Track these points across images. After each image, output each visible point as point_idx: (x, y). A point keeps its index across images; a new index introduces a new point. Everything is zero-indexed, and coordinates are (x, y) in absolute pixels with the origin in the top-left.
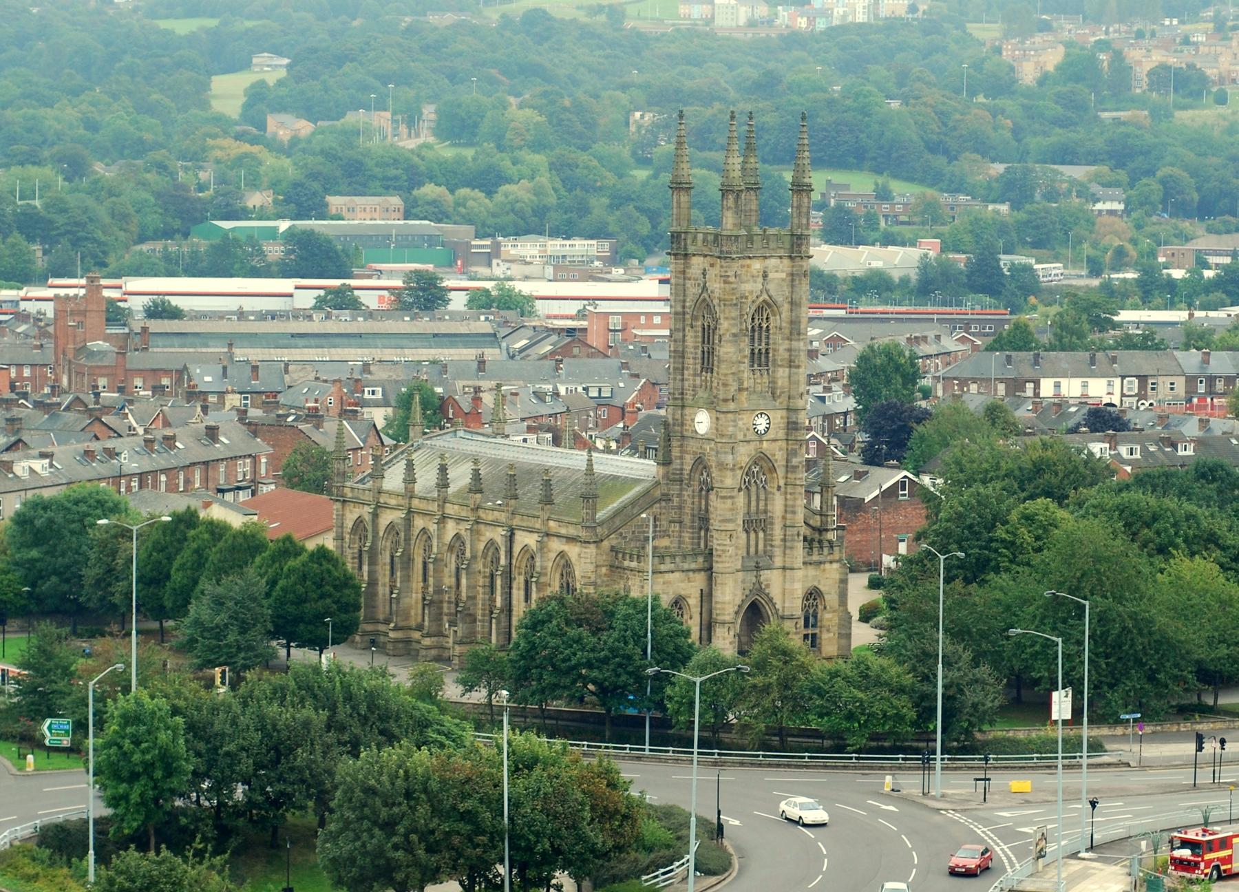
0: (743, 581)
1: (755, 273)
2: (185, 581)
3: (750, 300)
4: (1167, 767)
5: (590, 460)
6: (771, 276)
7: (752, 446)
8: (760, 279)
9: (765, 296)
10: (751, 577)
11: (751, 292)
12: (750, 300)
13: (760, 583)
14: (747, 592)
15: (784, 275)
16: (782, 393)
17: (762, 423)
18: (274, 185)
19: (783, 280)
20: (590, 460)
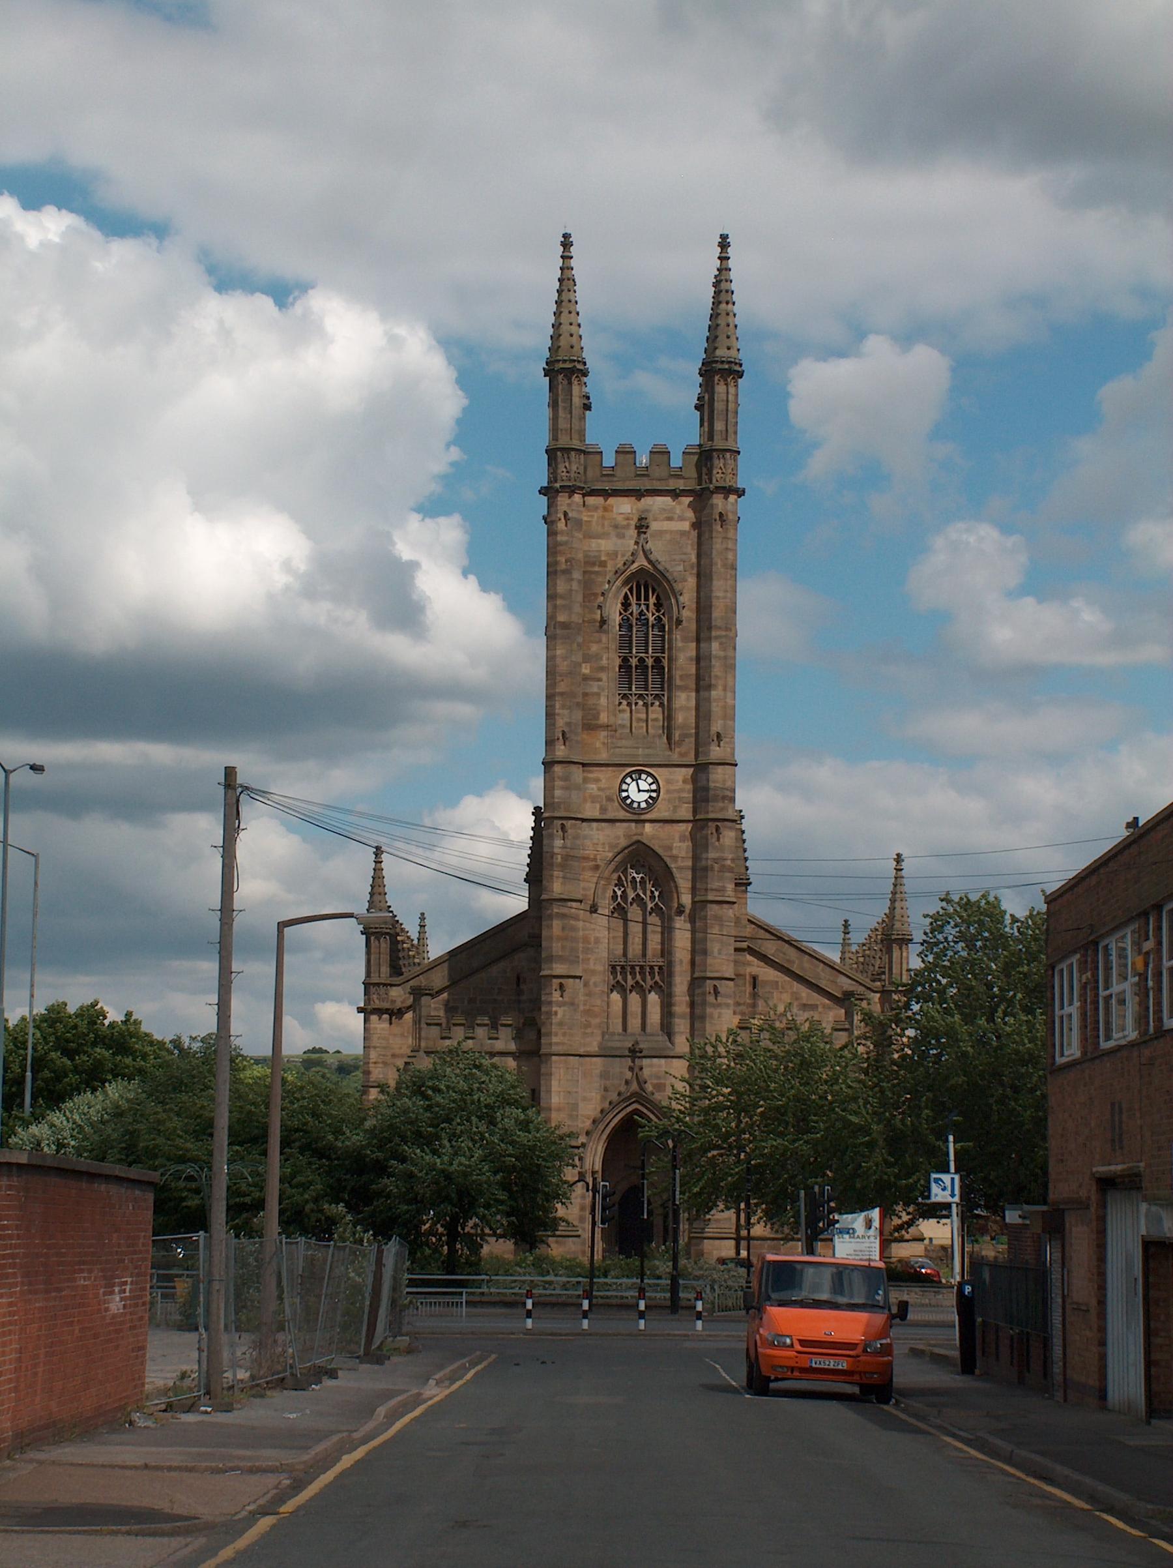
0: (604, 1075)
1: (620, 520)
2: (712, 854)
3: (610, 567)
4: (925, 1326)
5: (647, 713)
6: (655, 526)
7: (620, 829)
8: (633, 532)
9: (641, 562)
10: (621, 1068)
11: (614, 555)
12: (610, 567)
13: (641, 1083)
14: (614, 1097)
15: (686, 526)
16: (684, 736)
17: (638, 792)
18: (165, 1246)
19: (683, 533)
20: (647, 713)
